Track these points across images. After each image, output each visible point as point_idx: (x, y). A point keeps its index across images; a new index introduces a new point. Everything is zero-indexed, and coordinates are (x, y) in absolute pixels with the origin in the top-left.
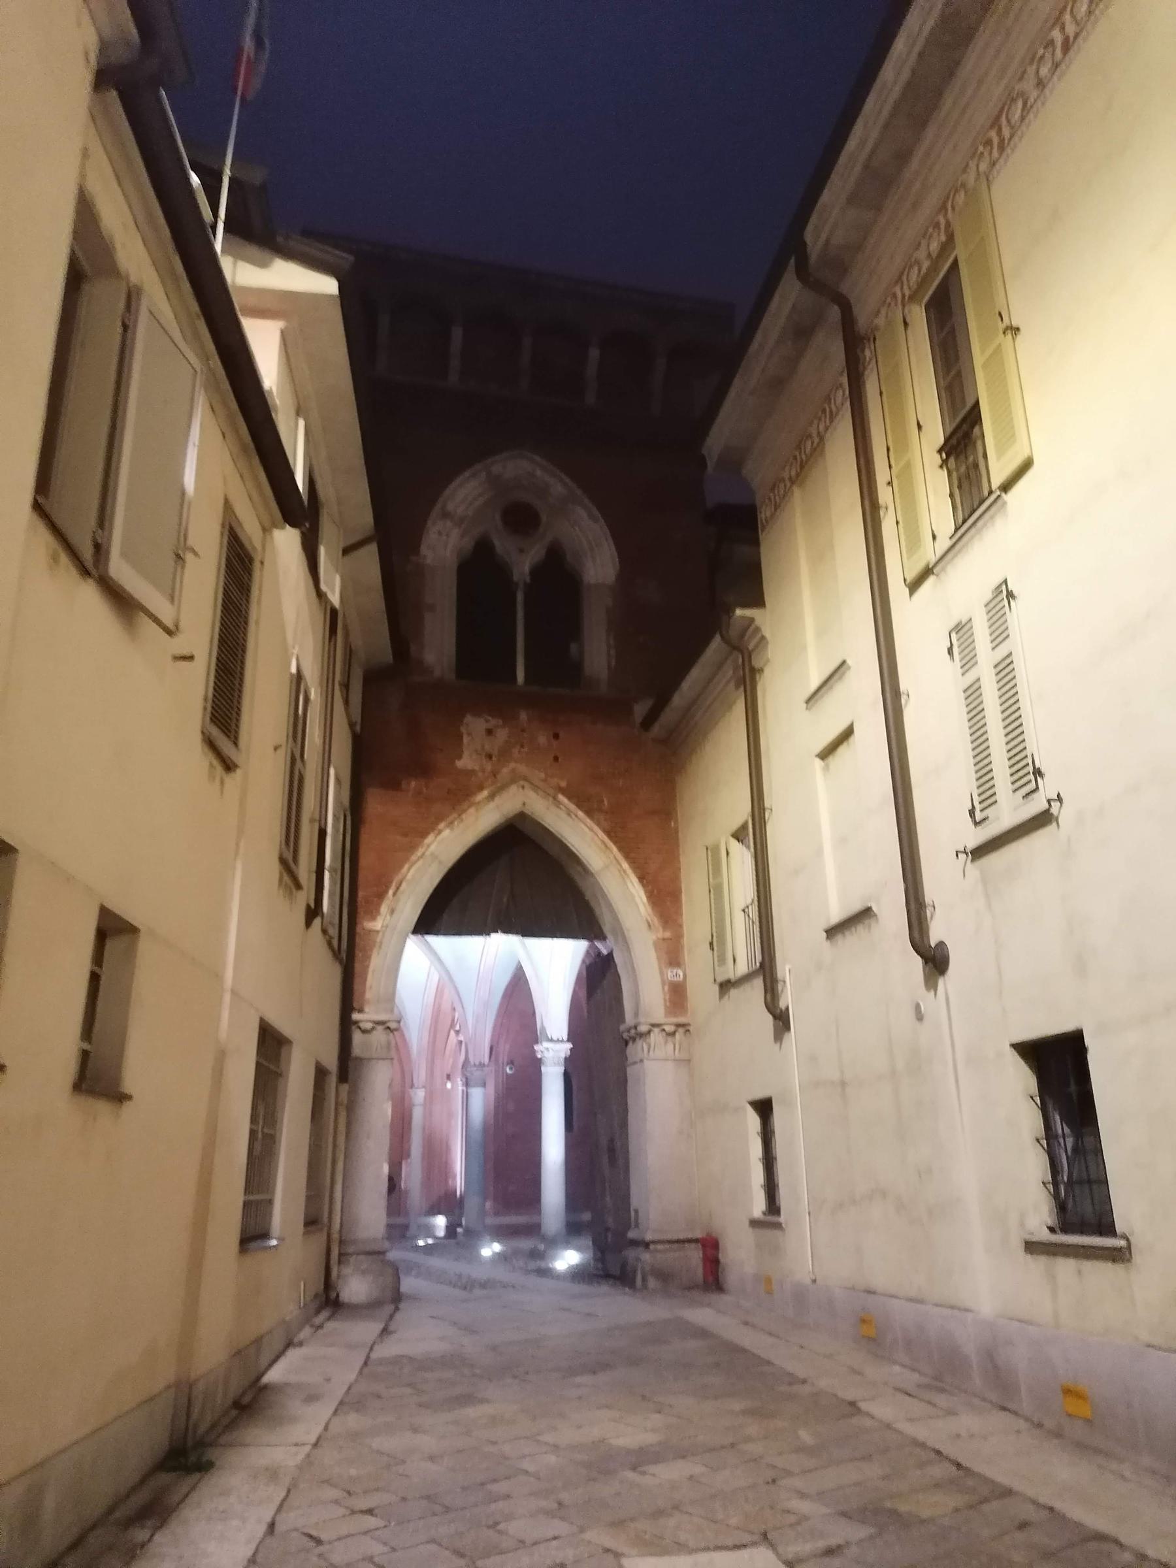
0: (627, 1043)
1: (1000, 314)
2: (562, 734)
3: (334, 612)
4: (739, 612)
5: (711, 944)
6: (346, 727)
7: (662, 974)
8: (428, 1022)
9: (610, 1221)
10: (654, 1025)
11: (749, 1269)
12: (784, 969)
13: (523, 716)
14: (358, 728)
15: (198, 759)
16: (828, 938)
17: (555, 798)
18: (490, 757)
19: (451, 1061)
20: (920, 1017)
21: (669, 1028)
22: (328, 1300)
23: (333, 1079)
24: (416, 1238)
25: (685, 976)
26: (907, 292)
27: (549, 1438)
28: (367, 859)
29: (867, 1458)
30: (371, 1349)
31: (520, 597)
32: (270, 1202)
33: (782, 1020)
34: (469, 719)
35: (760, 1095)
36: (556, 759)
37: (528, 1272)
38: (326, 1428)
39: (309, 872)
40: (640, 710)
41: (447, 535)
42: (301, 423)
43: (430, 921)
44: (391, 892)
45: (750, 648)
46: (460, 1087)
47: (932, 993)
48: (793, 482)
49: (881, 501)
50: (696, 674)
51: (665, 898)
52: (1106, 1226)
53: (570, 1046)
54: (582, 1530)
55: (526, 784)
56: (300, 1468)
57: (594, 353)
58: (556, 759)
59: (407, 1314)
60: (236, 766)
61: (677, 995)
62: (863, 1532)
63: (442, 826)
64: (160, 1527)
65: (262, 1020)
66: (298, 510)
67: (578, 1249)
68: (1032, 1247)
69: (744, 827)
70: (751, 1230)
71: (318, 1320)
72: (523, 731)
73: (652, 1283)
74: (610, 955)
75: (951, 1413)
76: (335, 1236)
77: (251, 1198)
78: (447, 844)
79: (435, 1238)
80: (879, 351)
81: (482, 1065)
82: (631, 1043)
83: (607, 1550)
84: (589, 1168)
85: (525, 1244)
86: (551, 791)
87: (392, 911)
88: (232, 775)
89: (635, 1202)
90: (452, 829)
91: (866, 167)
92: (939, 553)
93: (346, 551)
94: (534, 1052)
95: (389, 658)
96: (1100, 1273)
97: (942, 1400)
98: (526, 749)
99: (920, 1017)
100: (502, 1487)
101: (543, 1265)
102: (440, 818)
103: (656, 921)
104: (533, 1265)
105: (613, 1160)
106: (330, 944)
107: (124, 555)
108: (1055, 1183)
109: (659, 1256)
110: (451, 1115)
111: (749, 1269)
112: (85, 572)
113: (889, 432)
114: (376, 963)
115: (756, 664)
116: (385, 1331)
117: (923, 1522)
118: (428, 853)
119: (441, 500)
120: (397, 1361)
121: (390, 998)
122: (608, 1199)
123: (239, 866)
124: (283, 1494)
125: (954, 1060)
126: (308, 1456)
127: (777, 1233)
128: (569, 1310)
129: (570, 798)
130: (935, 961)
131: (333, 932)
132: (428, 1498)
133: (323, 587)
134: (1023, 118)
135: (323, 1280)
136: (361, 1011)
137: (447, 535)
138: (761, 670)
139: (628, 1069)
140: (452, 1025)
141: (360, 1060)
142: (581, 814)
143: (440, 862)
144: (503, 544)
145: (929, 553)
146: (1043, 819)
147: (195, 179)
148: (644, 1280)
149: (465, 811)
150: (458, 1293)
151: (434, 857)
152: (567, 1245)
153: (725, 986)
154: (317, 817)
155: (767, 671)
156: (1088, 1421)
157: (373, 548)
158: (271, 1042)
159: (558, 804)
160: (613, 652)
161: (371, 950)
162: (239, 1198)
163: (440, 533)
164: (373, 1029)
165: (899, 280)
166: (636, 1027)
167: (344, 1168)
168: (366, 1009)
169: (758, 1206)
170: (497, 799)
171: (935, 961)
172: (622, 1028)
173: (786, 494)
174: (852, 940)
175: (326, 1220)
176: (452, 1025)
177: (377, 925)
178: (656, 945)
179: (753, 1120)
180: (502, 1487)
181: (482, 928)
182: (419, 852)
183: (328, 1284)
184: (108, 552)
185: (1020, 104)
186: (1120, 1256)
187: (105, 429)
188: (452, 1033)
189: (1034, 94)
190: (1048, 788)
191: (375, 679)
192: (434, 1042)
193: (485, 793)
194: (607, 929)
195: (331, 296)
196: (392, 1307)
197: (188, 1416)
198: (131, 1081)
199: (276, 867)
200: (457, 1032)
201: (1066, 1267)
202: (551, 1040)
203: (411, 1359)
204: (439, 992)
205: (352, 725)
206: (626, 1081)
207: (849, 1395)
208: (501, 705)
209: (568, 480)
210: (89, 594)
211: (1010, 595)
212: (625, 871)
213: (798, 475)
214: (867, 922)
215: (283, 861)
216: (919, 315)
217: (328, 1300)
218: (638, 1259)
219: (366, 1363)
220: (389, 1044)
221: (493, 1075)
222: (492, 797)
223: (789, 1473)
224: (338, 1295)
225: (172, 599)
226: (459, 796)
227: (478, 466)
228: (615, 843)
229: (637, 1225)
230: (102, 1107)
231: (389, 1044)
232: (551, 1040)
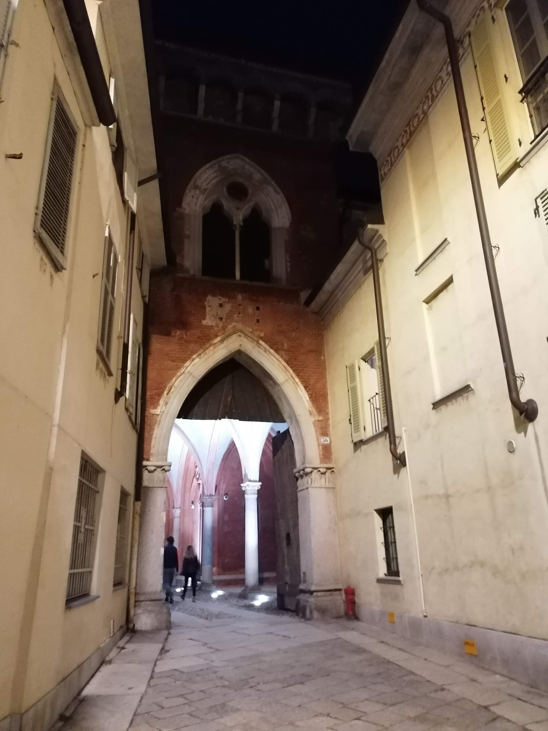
0: (297, 479)
2: (261, 307)
4: (370, 226)
5: (350, 420)
7: (318, 440)
9: (288, 579)
10: (315, 468)
11: (377, 608)
12: (400, 429)
13: (240, 297)
14: (147, 299)
15: (29, 253)
16: (434, 408)
17: (258, 343)
18: (221, 319)
19: (194, 494)
20: (511, 450)
21: (322, 470)
23: (131, 499)
28: (151, 374)
30: (155, 665)
31: (237, 233)
32: (90, 572)
33: (400, 461)
34: (209, 298)
36: (258, 321)
37: (240, 607)
39: (118, 369)
40: (304, 295)
43: (186, 412)
44: (165, 393)
45: (376, 247)
46: (199, 508)
47: (523, 434)
48: (403, 146)
49: (474, 132)
50: (340, 268)
51: (319, 398)
53: (260, 483)
55: (241, 334)
57: (277, 103)
58: (258, 321)
60: (63, 268)
65: (83, 452)
66: (105, 114)
67: (266, 593)
69: (371, 352)
70: (377, 584)
71: (121, 643)
72: (240, 305)
73: (316, 614)
76: (133, 591)
77: (76, 571)
78: (197, 367)
80: (473, 43)
81: (211, 495)
82: (300, 479)
84: (268, 547)
85: (238, 590)
86: (256, 339)
87: (166, 404)
88: (60, 273)
89: (303, 569)
90: (200, 358)
91: (412, 30)
93: (140, 183)
95: (164, 263)
98: (241, 315)
99: (511, 450)
102: (193, 353)
103: (314, 411)
105: (289, 543)
109: (319, 599)
110: (194, 523)
111: (377, 608)
113: (482, 86)
114: (157, 433)
115: (379, 257)
116: (163, 651)
118: (186, 371)
122: (286, 566)
123: (65, 341)
127: (398, 587)
128: (271, 633)
129: (266, 342)
131: (132, 410)
134: (441, 89)
135: (126, 613)
137: (197, 198)
138: (382, 260)
139: (299, 494)
142: (272, 351)
144: (228, 205)
148: (311, 612)
150: (202, 621)
153: (358, 445)
154: (123, 336)
155: (385, 260)
158: (89, 470)
160: (289, 264)
161: (154, 425)
162: (66, 572)
163: (193, 197)
164: (155, 470)
166: (303, 470)
167: (138, 551)
168: (151, 459)
169: (382, 570)
170: (225, 342)
172: (295, 471)
173: (399, 154)
177: (158, 411)
178: (314, 423)
179: (378, 521)
182: (182, 370)
183: (128, 620)
185: (440, 82)
188: (195, 480)
191: (156, 275)
192: (185, 485)
193: (219, 339)
194: (286, 416)
196: (165, 633)
199: (94, 357)
200: (198, 479)
204: (188, 459)
205: (143, 297)
206: (297, 501)
208: (227, 291)
209: (262, 171)
212: (297, 383)
213: (408, 141)
214: (465, 395)
215: (99, 352)
216: (502, 16)
217: (129, 629)
218: (308, 601)
219: (152, 677)
220: (164, 478)
221: (217, 501)
222: (222, 341)
224: (134, 625)
226: (204, 340)
227: (214, 162)
229: (305, 582)
231: (164, 478)
232: (250, 481)
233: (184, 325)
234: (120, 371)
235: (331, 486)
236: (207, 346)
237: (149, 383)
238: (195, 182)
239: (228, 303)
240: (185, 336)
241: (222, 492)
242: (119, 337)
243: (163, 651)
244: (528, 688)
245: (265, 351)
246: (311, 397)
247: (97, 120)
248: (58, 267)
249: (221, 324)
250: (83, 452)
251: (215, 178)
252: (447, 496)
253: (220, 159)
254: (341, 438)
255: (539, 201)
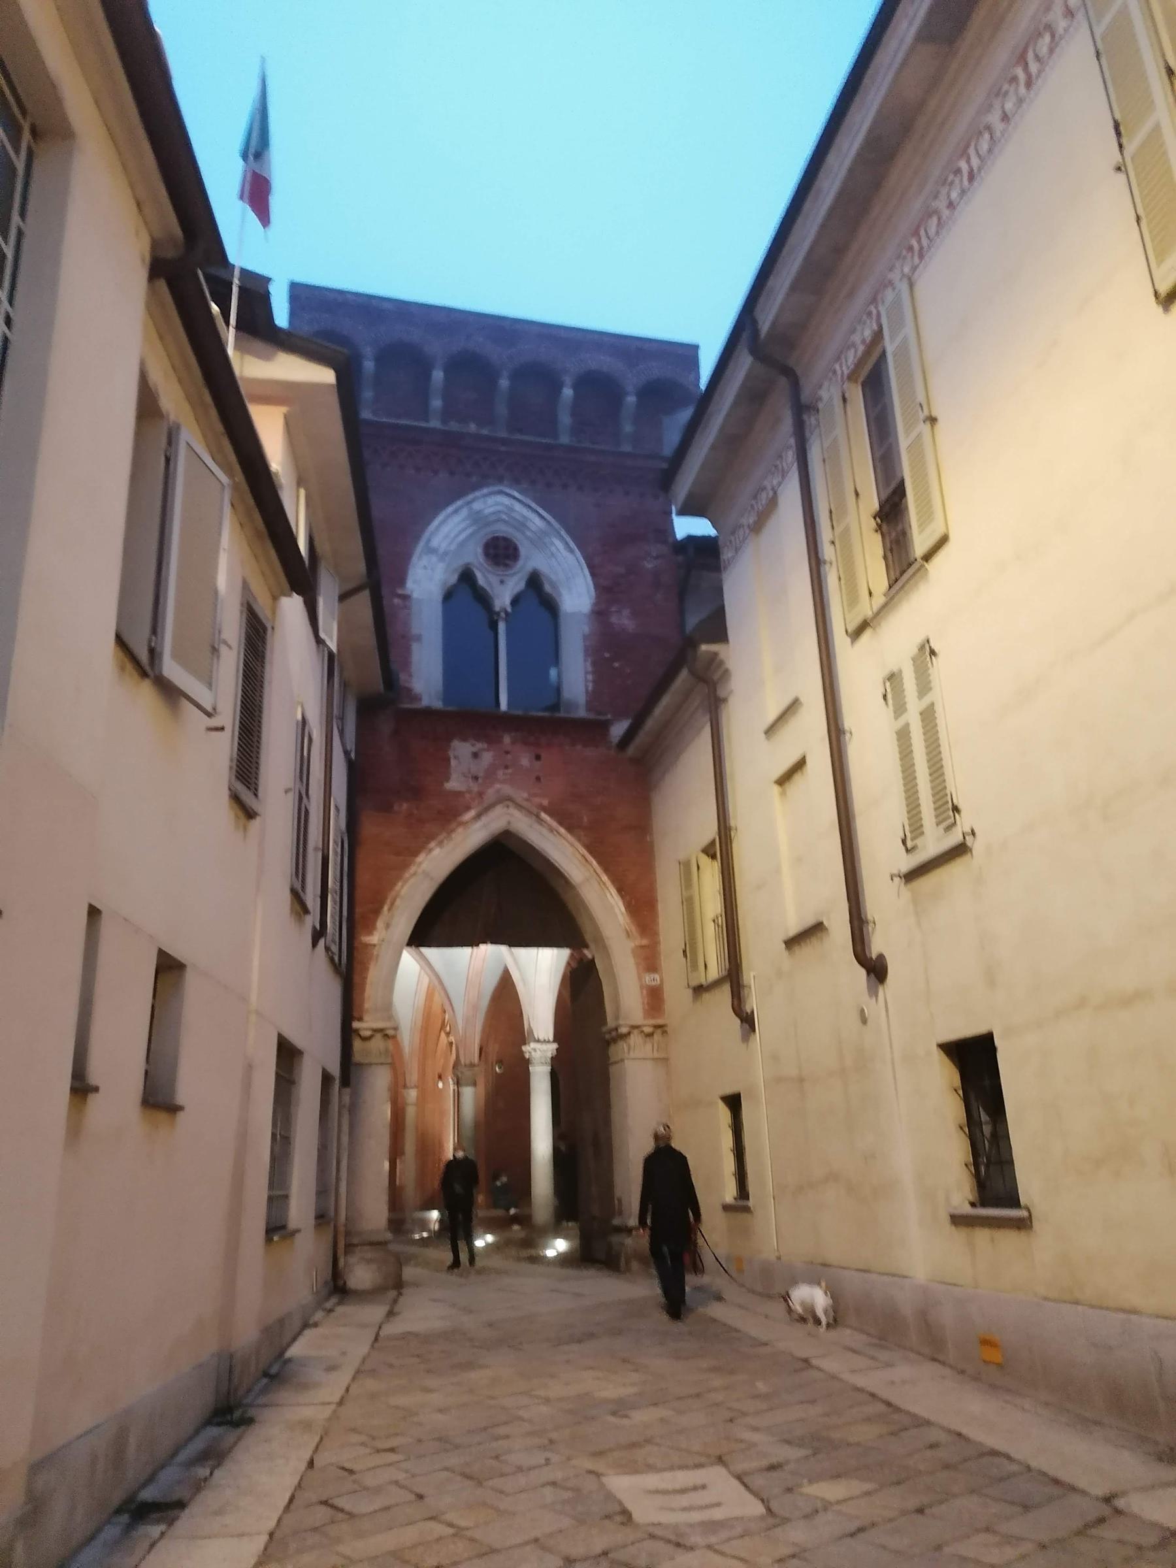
1: (921, 405)
2: (543, 755)
3: (331, 655)
5: (684, 952)
6: (342, 755)
8: (419, 1023)
12: (751, 975)
13: (507, 739)
14: (353, 755)
15: (222, 811)
17: (538, 816)
18: (476, 778)
20: (864, 1021)
21: (647, 1030)
22: (337, 1288)
24: (413, 1233)
25: (662, 980)
26: (846, 372)
27: (542, 1393)
28: (364, 878)
29: (813, 1402)
32: (286, 1197)
33: (748, 1021)
35: (729, 1090)
36: (538, 779)
37: (519, 1259)
38: (347, 1390)
40: (618, 730)
41: (432, 569)
42: (302, 492)
43: (424, 934)
44: (386, 908)
46: (452, 1087)
51: (642, 908)
52: (1015, 1202)
53: (555, 1046)
54: (569, 1459)
56: (329, 1419)
58: (538, 779)
59: (409, 1297)
61: (655, 998)
62: (802, 1452)
63: (432, 844)
64: (219, 1465)
65: (280, 1036)
66: (300, 576)
67: (565, 1238)
68: (958, 1220)
69: (713, 843)
71: (328, 1305)
72: (507, 753)
74: (593, 961)
75: (888, 1365)
76: (342, 1229)
78: (439, 860)
79: (429, 1231)
81: (472, 1065)
83: (590, 1472)
86: (535, 810)
87: (388, 926)
92: (875, 609)
94: (522, 1052)
96: (1009, 1239)
97: (884, 1356)
98: (510, 771)
99: (864, 1021)
100: (502, 1431)
101: (533, 1252)
102: (431, 837)
103: (633, 929)
104: (525, 1253)
106: (332, 960)
107: (175, 656)
108: (976, 1164)
112: (144, 674)
114: (374, 975)
115: (721, 693)
116: (391, 1314)
117: (849, 1445)
119: (426, 535)
120: (405, 1336)
121: (387, 1008)
124: (317, 1439)
125: (893, 1059)
126: (335, 1411)
127: (745, 1215)
130: (876, 970)
131: (335, 948)
132: (440, 1439)
133: (322, 635)
134: (937, 233)
136: (360, 1019)
138: (725, 700)
140: (443, 1026)
141: (360, 1065)
142: (562, 830)
143: (432, 879)
145: (866, 609)
146: (960, 850)
147: (215, 308)
148: (627, 1262)
149: (453, 831)
151: (426, 874)
152: (558, 1233)
153: (699, 990)
156: (1000, 1366)
157: (366, 594)
158: (287, 1054)
159: (540, 821)
160: (590, 677)
163: (425, 567)
165: (838, 358)
166: (616, 1029)
168: (366, 1018)
169: (730, 1193)
171: (876, 970)
172: (604, 1029)
174: (806, 951)
175: (332, 1213)
176: (443, 1026)
177: (374, 939)
178: (634, 951)
179: (724, 1114)
180: (502, 1431)
181: (473, 942)
182: (413, 869)
184: (161, 654)
186: (1023, 1225)
187: (154, 547)
188: (443, 1034)
189: (946, 213)
190: (965, 822)
193: (472, 813)
194: (588, 937)
195: (330, 385)
196: (392, 1294)
197: (230, 1380)
198: (181, 1098)
199: (287, 895)
200: (448, 1034)
201: (982, 1236)
202: (538, 1041)
203: (416, 1335)
205: (346, 753)
207: (804, 1355)
210: (146, 691)
211: (933, 653)
216: (857, 395)
218: (623, 1244)
219: (376, 1339)
222: (478, 816)
223: (744, 1414)
224: (345, 1283)
225: (210, 685)
226: (448, 815)
227: (459, 503)
228: (595, 857)
229: (621, 1213)
230: (162, 1116)
232: (538, 1041)
233: (416, 793)
234: (319, 900)
235: (663, 1055)
236: (453, 825)
237: (359, 894)
238: (429, 540)
239: (488, 750)
240: (415, 812)
241: (493, 1057)
242: (316, 849)
243: (391, 1314)
244: (877, 1341)
245: (551, 830)
246: (628, 906)
247: (286, 586)
248: (250, 815)
249: (475, 788)
250: (280, 1036)
251: (464, 530)
252: (801, 1080)
253: (470, 497)
254: (674, 977)
255: (888, 684)
